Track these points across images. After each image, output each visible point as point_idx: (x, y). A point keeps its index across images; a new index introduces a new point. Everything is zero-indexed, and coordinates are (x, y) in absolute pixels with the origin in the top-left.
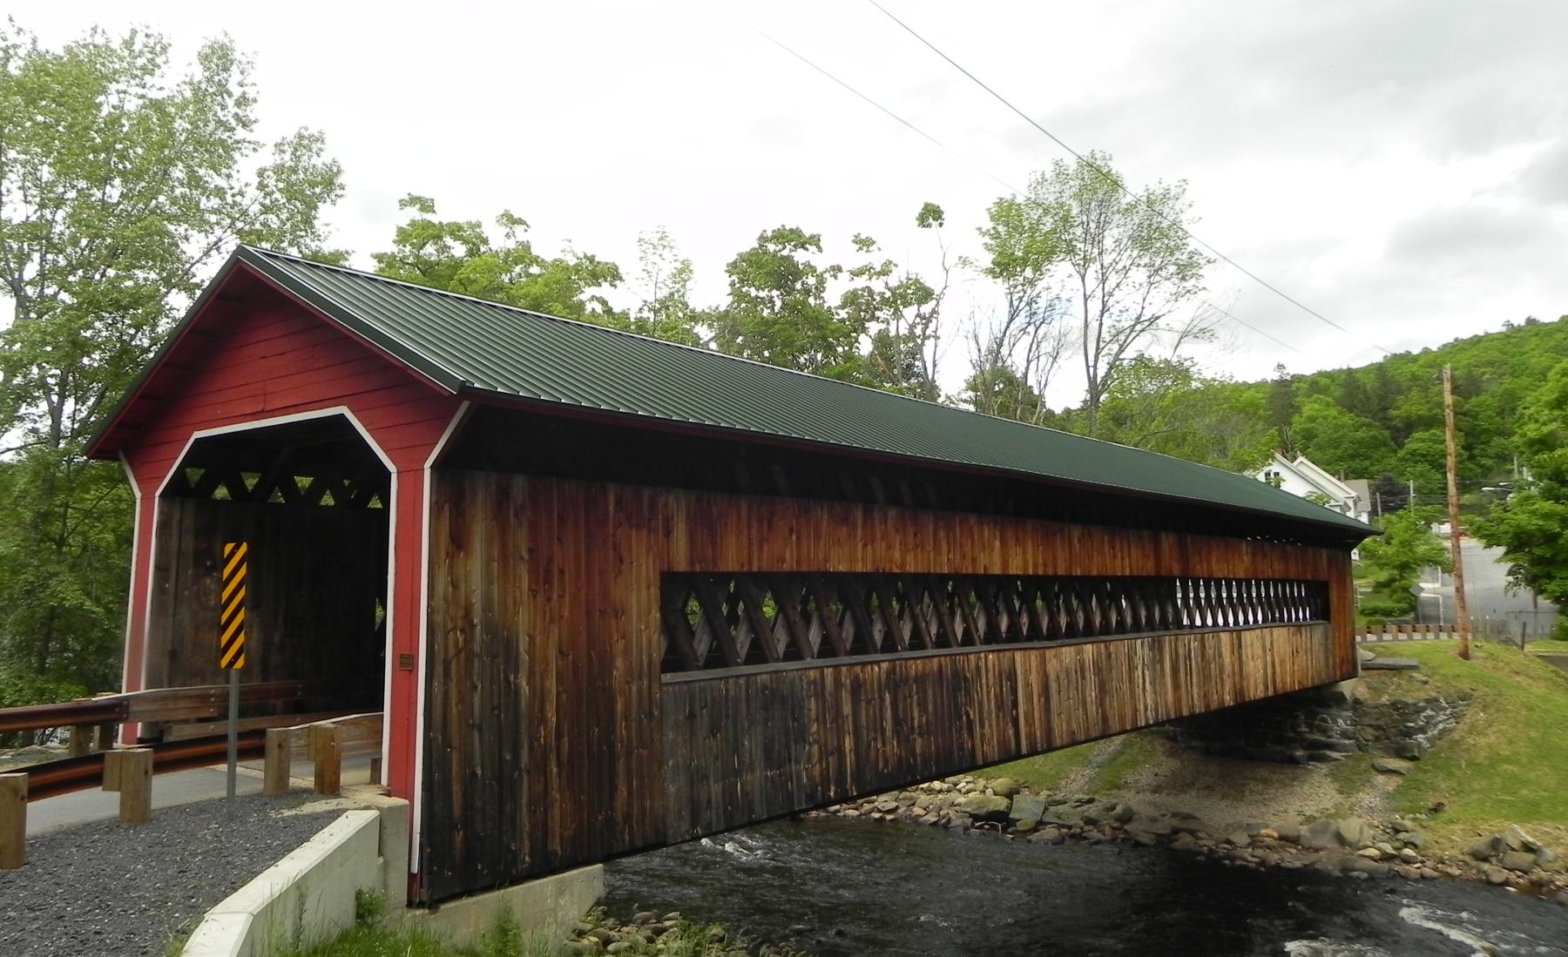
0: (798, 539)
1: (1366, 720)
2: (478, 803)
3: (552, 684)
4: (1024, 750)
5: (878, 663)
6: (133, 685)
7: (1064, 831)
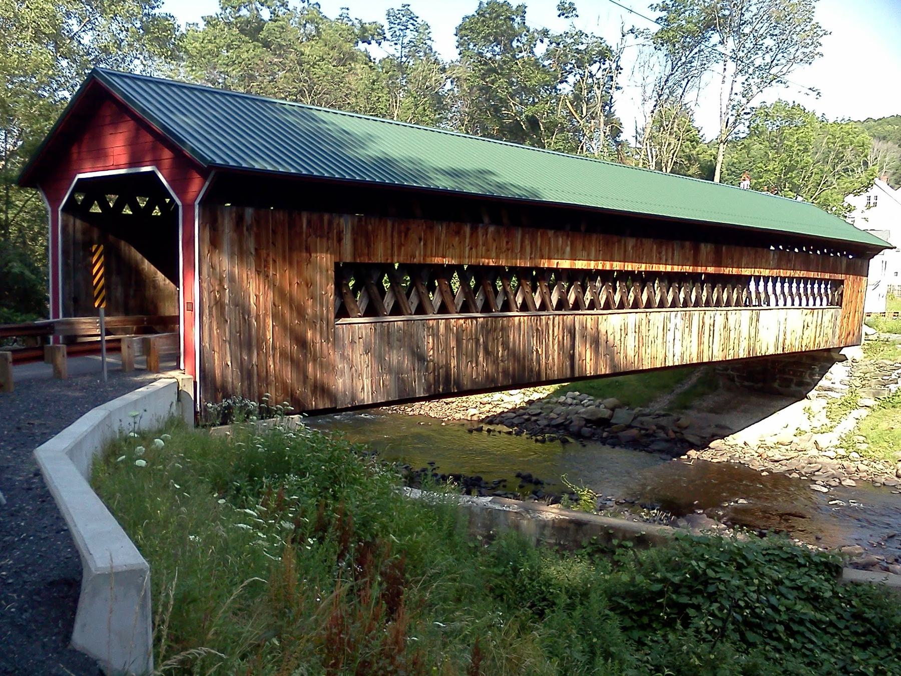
0: (425, 244)
5: (476, 318)
6: (56, 315)
7: (643, 432)
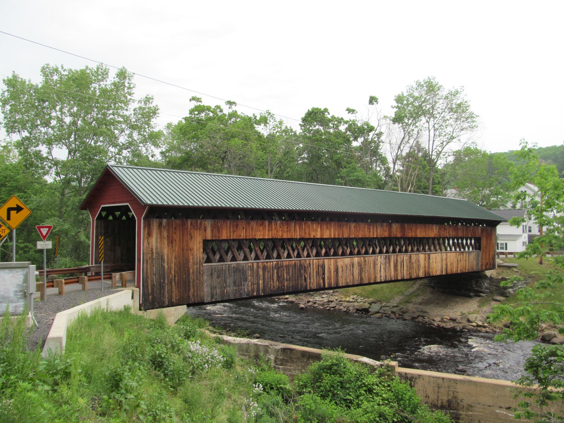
0: (246, 230)
1: (494, 284)
2: (155, 290)
3: (173, 265)
4: (327, 286)
5: (272, 262)
6: (92, 264)
